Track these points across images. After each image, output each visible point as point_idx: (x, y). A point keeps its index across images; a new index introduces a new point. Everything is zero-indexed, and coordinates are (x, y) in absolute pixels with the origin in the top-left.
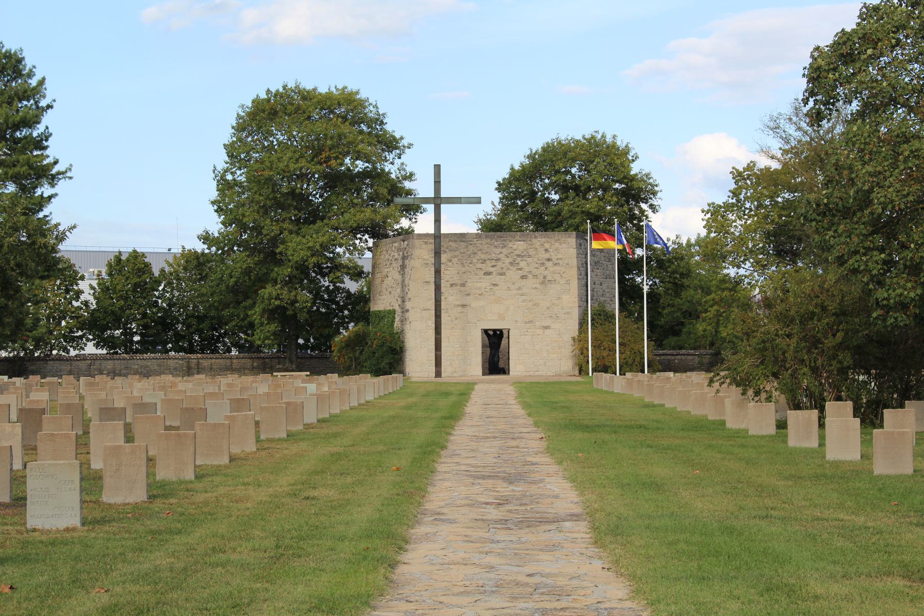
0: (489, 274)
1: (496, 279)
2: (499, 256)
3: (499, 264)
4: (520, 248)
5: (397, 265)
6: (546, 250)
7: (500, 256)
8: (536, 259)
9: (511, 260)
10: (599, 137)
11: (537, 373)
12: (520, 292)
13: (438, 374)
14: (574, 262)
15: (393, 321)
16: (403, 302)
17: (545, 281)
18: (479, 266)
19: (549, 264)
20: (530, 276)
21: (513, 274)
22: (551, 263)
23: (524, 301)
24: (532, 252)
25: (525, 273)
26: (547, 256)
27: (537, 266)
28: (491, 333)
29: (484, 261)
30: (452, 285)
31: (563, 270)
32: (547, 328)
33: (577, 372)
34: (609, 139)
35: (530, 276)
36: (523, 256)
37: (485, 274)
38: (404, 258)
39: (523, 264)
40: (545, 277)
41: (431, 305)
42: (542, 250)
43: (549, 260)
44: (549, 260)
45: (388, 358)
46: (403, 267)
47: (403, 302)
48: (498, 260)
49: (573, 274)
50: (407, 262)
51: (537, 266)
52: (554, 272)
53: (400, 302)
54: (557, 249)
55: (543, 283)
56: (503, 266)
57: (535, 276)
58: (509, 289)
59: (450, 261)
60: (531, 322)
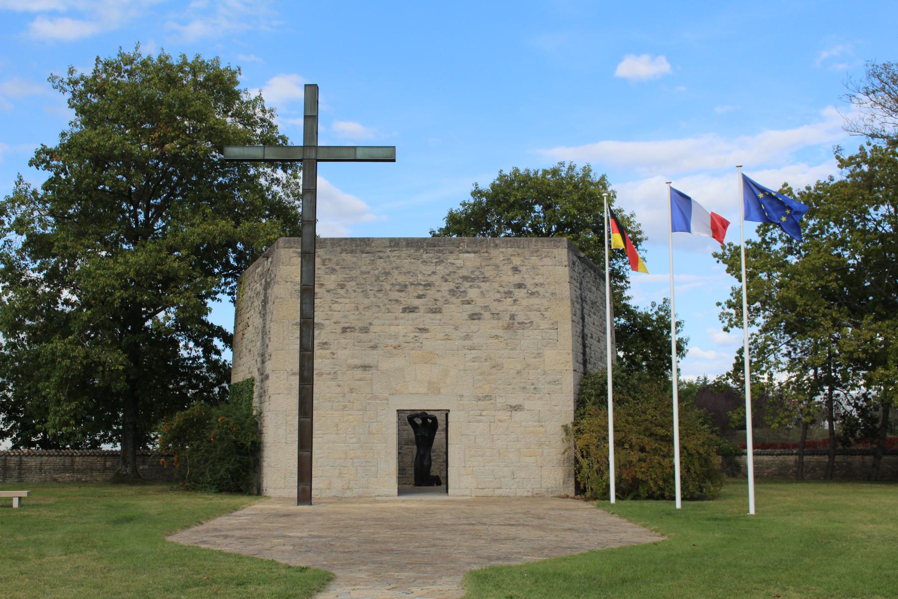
1: (423, 318)
2: (430, 279)
3: (432, 293)
4: (468, 264)
5: (258, 303)
6: (516, 269)
7: (433, 279)
8: (496, 285)
9: (451, 285)
10: (565, 169)
11: (498, 492)
12: (467, 343)
13: (305, 496)
15: (251, 398)
16: (263, 362)
17: (513, 325)
18: (395, 295)
19: (520, 294)
21: (455, 311)
22: (523, 291)
23: (474, 360)
24: (489, 272)
25: (478, 310)
26: (517, 279)
27: (498, 296)
29: (403, 288)
30: (344, 330)
32: (517, 408)
33: (571, 491)
35: (487, 315)
36: (473, 280)
37: (404, 310)
39: (473, 293)
40: (512, 317)
42: (507, 269)
43: (520, 286)
44: (520, 286)
45: (239, 470)
46: (265, 302)
47: (263, 362)
48: (428, 285)
50: (269, 291)
51: (498, 296)
52: (529, 308)
53: (259, 365)
54: (534, 267)
55: (509, 327)
56: (438, 296)
57: (496, 316)
58: (447, 338)
59: (342, 286)
60: (487, 397)
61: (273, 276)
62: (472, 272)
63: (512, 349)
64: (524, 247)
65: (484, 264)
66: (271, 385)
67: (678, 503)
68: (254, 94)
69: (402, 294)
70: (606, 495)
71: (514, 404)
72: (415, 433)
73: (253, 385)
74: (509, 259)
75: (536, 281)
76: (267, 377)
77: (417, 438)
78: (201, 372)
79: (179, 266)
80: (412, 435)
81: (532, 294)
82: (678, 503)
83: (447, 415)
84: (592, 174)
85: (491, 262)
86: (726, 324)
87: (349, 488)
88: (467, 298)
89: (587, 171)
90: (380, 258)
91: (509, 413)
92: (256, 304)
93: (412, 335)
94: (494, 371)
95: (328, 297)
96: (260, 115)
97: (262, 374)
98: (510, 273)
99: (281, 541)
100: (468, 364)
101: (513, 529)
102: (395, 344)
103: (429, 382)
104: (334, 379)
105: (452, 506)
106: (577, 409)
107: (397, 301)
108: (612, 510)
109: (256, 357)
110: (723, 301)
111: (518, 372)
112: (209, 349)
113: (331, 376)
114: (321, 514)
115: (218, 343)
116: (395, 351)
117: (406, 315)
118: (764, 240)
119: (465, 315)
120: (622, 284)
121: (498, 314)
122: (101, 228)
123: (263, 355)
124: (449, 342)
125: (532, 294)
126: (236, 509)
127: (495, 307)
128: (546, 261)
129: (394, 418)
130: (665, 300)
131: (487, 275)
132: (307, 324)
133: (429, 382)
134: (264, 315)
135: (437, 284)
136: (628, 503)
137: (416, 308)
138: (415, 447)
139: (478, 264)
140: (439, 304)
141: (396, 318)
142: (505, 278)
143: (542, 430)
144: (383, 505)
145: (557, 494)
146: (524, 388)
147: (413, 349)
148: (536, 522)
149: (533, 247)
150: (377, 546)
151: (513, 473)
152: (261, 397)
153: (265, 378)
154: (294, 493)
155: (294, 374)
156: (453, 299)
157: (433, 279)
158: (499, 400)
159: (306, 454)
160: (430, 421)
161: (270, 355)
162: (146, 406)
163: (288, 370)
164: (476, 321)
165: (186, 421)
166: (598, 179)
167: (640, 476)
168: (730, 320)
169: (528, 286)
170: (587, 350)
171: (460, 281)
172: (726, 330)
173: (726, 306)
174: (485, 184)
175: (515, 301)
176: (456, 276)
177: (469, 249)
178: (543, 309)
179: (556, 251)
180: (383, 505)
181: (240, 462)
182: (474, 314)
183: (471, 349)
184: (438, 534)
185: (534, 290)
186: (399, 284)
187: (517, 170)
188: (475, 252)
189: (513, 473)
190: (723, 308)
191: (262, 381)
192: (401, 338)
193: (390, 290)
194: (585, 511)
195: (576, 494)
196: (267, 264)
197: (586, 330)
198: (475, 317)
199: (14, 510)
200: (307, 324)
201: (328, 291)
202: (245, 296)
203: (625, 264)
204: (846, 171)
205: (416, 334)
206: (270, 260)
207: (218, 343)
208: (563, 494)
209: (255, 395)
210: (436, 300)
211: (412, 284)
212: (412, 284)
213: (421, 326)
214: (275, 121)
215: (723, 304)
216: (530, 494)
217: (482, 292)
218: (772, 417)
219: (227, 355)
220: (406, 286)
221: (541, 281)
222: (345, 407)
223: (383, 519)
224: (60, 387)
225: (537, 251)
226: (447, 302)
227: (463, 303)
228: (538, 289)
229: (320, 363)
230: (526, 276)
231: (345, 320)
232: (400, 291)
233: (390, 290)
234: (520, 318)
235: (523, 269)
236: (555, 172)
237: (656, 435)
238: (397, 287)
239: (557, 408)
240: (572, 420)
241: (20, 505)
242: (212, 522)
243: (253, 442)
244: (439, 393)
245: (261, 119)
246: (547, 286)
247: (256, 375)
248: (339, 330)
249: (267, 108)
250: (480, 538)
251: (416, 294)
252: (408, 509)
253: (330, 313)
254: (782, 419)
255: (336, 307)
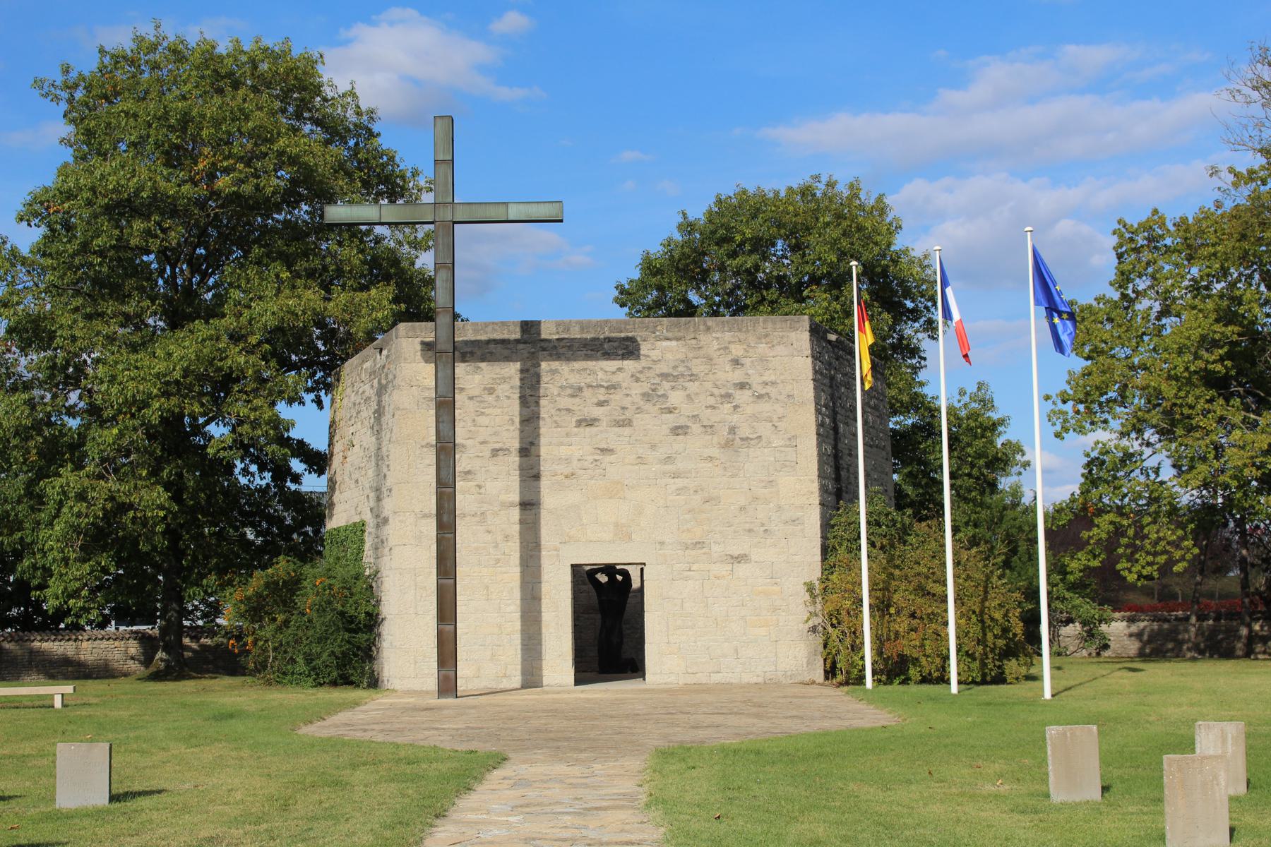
0: (590, 422)
2: (615, 379)
3: (617, 397)
4: (669, 356)
5: (367, 413)
6: (736, 362)
7: (619, 378)
8: (709, 385)
9: (646, 387)
10: (822, 186)
11: (716, 678)
13: (448, 686)
14: (806, 390)
15: (360, 550)
16: (379, 499)
17: (733, 441)
18: (565, 402)
19: (743, 397)
20: (696, 428)
21: (652, 423)
22: (747, 393)
23: (680, 491)
24: (699, 367)
25: (682, 421)
26: (738, 376)
27: (711, 401)
28: (603, 578)
29: (577, 391)
30: (495, 453)
31: (780, 411)
32: (740, 559)
33: (819, 675)
34: (843, 189)
35: (696, 428)
36: (676, 377)
37: (579, 423)
38: (381, 390)
39: (676, 398)
40: (732, 430)
41: (430, 504)
42: (723, 362)
43: (742, 386)
44: (742, 386)
45: (349, 652)
46: (379, 413)
47: (379, 499)
48: (613, 387)
49: (803, 421)
50: (385, 398)
51: (711, 401)
52: (755, 417)
53: (372, 503)
54: (763, 359)
55: (728, 445)
56: (626, 402)
57: (709, 428)
58: (641, 460)
59: (491, 391)
60: (699, 544)
61: (390, 377)
62: (675, 367)
63: (732, 476)
64: (748, 331)
65: (691, 355)
66: (390, 531)
67: (954, 687)
68: (343, 87)
69: (577, 400)
70: (860, 680)
71: (736, 553)
72: (599, 596)
73: (363, 531)
74: (726, 348)
75: (765, 378)
76: (386, 521)
77: (601, 602)
78: (276, 511)
79: (246, 362)
80: (594, 599)
81: (760, 397)
82: (954, 687)
83: (642, 570)
84: (862, 196)
85: (702, 352)
86: (1058, 428)
87: (505, 676)
88: (668, 405)
89: (854, 188)
90: (544, 350)
91: (729, 567)
92: (364, 414)
93: (590, 458)
94: (707, 506)
95: (471, 406)
96: (354, 119)
97: (377, 516)
98: (728, 367)
99: (435, 732)
100: (671, 498)
101: (722, 717)
102: (568, 471)
103: (616, 525)
104: (483, 521)
105: (647, 696)
106: (824, 559)
107: (568, 410)
108: (870, 698)
109: (368, 491)
110: (1054, 392)
111: (742, 509)
112: (282, 473)
113: (477, 519)
114: (474, 707)
115: (297, 465)
116: (567, 482)
117: (581, 429)
118: (1124, 296)
119: (665, 429)
120: (914, 361)
121: (711, 427)
122: (123, 303)
123: (378, 490)
124: (642, 467)
125: (760, 397)
126: (357, 704)
127: (708, 417)
128: (780, 350)
129: (568, 577)
130: (980, 386)
131: (695, 371)
132: (446, 449)
133: (616, 525)
134: (377, 430)
135: (624, 385)
136: (896, 688)
137: (596, 420)
138: (599, 616)
139: (681, 356)
140: (628, 414)
141: (568, 435)
142: (720, 375)
143: (776, 588)
144: (555, 696)
145: (799, 679)
146: (750, 531)
147: (592, 478)
148: (754, 710)
149: (760, 330)
150: (552, 735)
151: (736, 650)
152: (377, 549)
153: (382, 522)
154: (432, 683)
155: (425, 516)
156: (648, 407)
157: (619, 378)
158: (715, 548)
159: (450, 628)
160: (619, 578)
161: (390, 490)
162: (225, 568)
163: (417, 510)
164: (681, 437)
165: (267, 585)
166: (872, 202)
167: (907, 652)
168: (1065, 421)
169: (754, 386)
170: (843, 473)
171: (657, 380)
172: (1058, 435)
173: (1059, 402)
174: (698, 213)
175: (736, 407)
176: (650, 374)
177: (670, 335)
178: (775, 418)
179: (793, 335)
180: (555, 696)
181: (349, 642)
182: (677, 428)
183: (675, 475)
184: (625, 723)
185: (763, 392)
186: (571, 387)
187: (744, 192)
188: (678, 339)
189: (736, 650)
190: (1054, 403)
191: (378, 526)
192: (575, 462)
193: (559, 395)
194: (837, 698)
195: (827, 678)
196: (381, 359)
197: (840, 446)
198: (680, 431)
199: (58, 711)
200: (446, 449)
201: (471, 398)
202: (346, 400)
203: (916, 332)
204: (1246, 190)
205: (597, 457)
206: (385, 352)
207: (297, 465)
208: (807, 679)
209: (368, 545)
210: (623, 408)
211: (589, 386)
212: (589, 386)
213: (603, 446)
214: (375, 128)
215: (1054, 397)
216: (760, 680)
217: (689, 396)
218: (1129, 565)
219: (312, 483)
220: (580, 389)
221: (773, 378)
222: (498, 561)
223: (556, 710)
224: (66, 541)
225: (766, 336)
226: (639, 410)
227: (663, 411)
228: (769, 389)
229: (464, 501)
230: (750, 372)
231: (495, 439)
232: (573, 396)
233: (559, 395)
234: (744, 431)
235: (747, 361)
236: (806, 192)
237: (934, 595)
238: (569, 391)
239: (797, 558)
240: (819, 575)
241: (64, 705)
242: (335, 717)
243: (368, 614)
244: (630, 538)
245: (355, 125)
246: (781, 386)
247: (368, 517)
248: (488, 454)
249: (363, 108)
250: (678, 726)
251: (596, 401)
252: (588, 700)
253: (473, 429)
254: (1143, 567)
255: (482, 420)
